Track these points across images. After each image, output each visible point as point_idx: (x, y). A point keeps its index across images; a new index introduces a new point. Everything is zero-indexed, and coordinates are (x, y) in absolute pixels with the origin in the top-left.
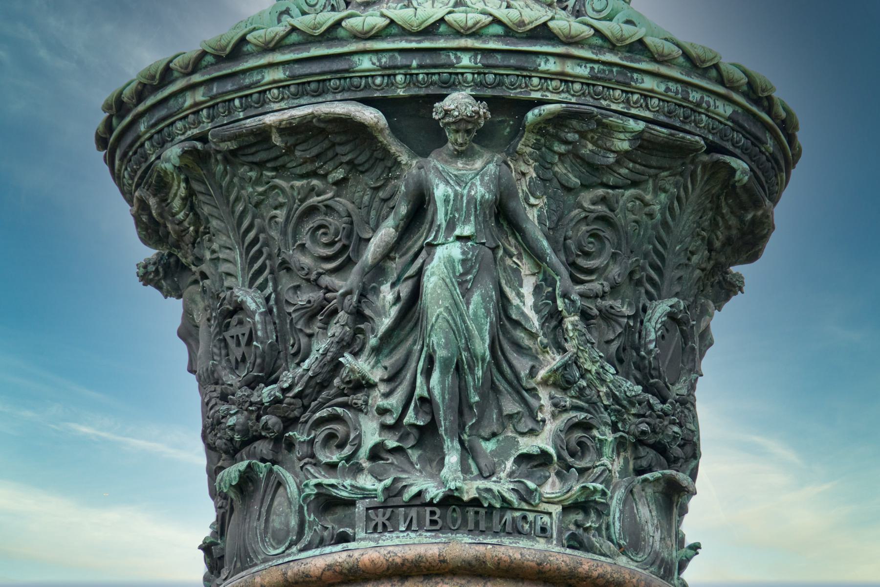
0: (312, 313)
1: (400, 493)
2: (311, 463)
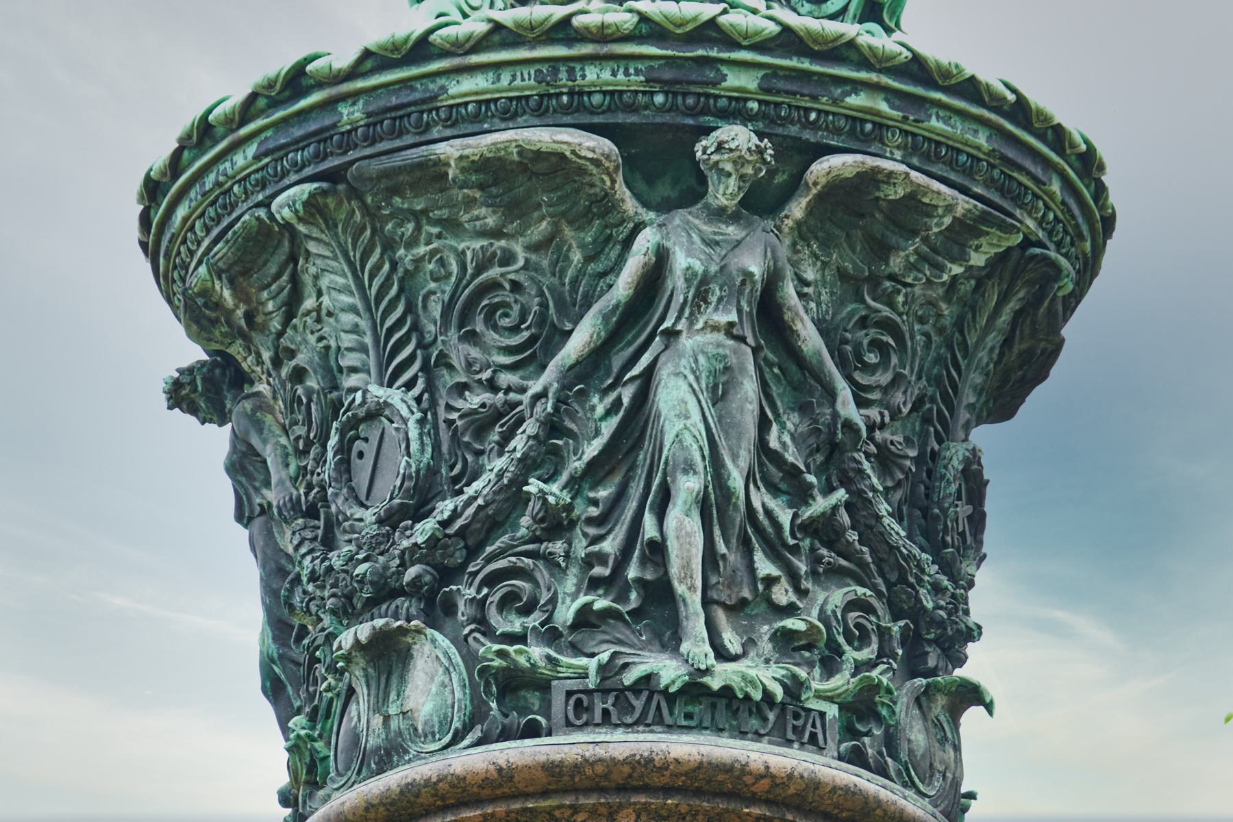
0: (482, 423)
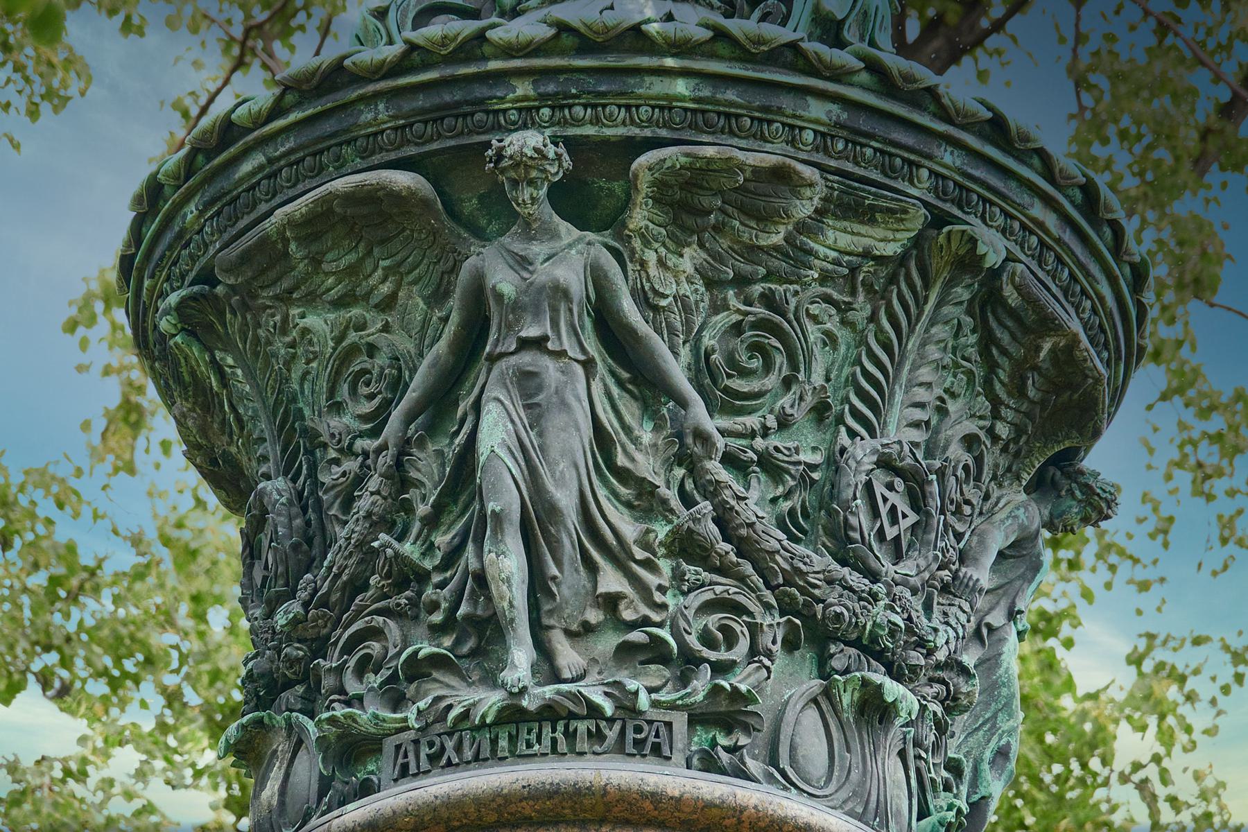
1: (442, 717)
2: (339, 701)
